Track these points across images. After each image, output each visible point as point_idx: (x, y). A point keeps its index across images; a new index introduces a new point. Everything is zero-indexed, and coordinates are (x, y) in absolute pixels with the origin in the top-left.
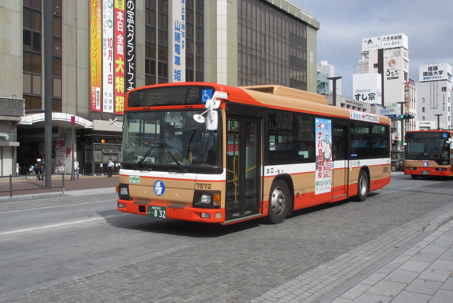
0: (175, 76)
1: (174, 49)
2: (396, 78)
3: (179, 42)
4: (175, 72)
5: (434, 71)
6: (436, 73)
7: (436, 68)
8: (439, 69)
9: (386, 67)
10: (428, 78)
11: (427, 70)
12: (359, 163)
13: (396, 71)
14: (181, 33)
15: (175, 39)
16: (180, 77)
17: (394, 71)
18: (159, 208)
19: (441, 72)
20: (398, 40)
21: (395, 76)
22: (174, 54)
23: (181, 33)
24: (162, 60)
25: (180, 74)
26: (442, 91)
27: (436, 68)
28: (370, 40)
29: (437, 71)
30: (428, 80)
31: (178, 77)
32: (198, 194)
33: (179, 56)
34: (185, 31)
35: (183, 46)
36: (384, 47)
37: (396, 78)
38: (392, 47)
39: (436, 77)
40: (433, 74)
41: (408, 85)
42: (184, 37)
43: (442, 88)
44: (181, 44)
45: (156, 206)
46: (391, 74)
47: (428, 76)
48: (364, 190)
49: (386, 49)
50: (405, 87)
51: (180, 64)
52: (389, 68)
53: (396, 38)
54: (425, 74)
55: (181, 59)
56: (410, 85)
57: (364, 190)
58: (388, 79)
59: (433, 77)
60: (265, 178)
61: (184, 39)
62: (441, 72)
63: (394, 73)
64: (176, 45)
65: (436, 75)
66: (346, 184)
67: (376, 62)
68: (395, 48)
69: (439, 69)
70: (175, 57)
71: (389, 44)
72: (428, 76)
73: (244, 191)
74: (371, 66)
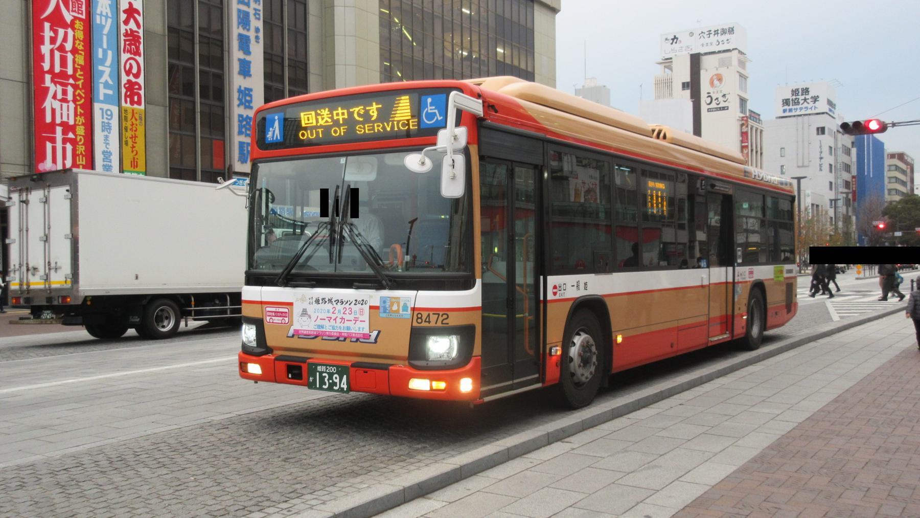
0: (239, 99)
1: (235, 44)
2: (723, 109)
3: (248, 30)
4: (240, 91)
5: (803, 97)
6: (805, 100)
7: (806, 91)
8: (812, 93)
9: (705, 87)
10: (790, 110)
11: (788, 95)
12: (751, 273)
13: (724, 96)
14: (252, 12)
15: (239, 23)
16: (251, 101)
17: (720, 96)
18: (333, 370)
19: (815, 99)
20: (727, 36)
21: (722, 105)
22: (236, 54)
23: (252, 12)
24: (209, 66)
25: (251, 96)
26: (818, 134)
27: (806, 91)
28: (675, 37)
29: (807, 97)
30: (790, 114)
31: (247, 101)
32: (418, 336)
33: (248, 58)
34: (261, 7)
35: (257, 38)
36: (702, 50)
37: (723, 109)
38: (717, 49)
39: (806, 108)
40: (801, 102)
41: (747, 121)
42: (259, 19)
43: (818, 129)
44: (252, 34)
45: (326, 365)
46: (714, 102)
47: (791, 107)
48: (755, 331)
49: (706, 54)
50: (742, 125)
51: (250, 76)
52: (711, 90)
53: (724, 32)
54: (786, 102)
55: (252, 65)
56: (751, 122)
57: (755, 331)
58: (709, 110)
59: (801, 109)
60: (549, 305)
61: (260, 24)
62: (815, 99)
63: (721, 99)
64: (240, 36)
65: (805, 105)
66: (730, 313)
67: (687, 79)
68: (725, 51)
69: (812, 93)
70: (239, 60)
71: (711, 44)
72: (791, 107)
73: (505, 333)
74: (677, 86)
